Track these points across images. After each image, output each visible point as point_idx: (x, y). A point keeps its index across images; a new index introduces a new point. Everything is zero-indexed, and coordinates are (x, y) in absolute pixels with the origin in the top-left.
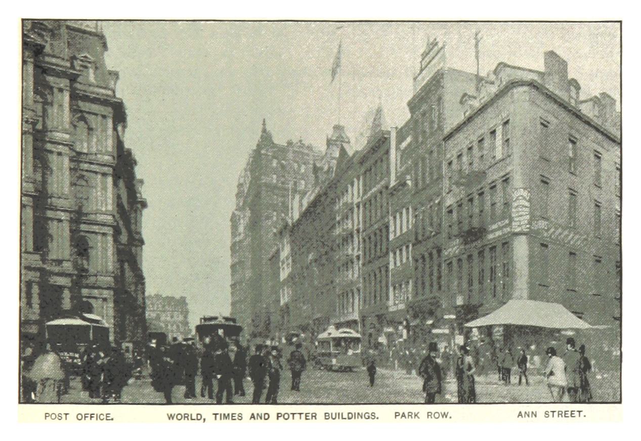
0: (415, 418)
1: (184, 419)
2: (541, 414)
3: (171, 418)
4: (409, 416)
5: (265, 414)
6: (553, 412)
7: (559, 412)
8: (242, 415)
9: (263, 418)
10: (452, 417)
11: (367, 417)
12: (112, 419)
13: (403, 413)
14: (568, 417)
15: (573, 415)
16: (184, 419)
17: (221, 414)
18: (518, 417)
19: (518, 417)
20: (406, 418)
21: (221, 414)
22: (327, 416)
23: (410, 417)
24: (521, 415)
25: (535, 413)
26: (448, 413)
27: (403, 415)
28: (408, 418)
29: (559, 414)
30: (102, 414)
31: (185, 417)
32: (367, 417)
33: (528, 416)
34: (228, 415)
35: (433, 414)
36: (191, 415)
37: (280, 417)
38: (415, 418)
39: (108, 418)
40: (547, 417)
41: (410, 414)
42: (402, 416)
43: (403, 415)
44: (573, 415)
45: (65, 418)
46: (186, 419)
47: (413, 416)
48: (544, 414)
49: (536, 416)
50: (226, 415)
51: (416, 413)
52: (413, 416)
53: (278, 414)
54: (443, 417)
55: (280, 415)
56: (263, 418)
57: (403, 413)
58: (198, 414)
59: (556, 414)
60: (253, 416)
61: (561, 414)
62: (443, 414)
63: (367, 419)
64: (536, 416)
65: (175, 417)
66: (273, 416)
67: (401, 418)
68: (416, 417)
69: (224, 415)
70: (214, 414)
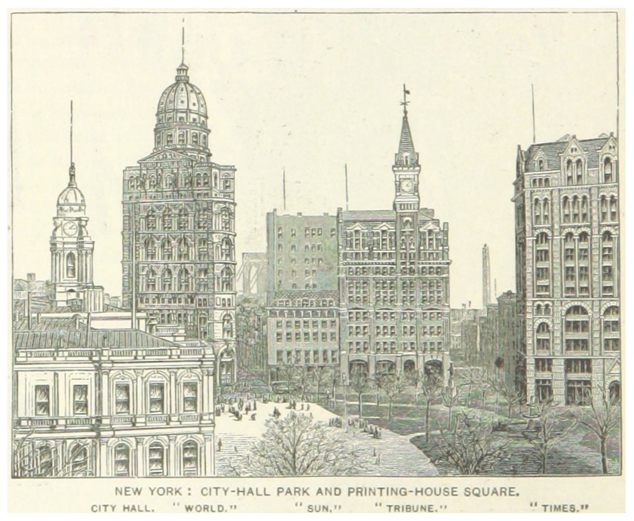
0: (303, 494)
1: (167, 494)
2: (460, 491)
3: (137, 493)
4: (295, 492)
5: (336, 489)
6: (381, 489)
7: (396, 506)
8: (465, 494)
9: (333, 493)
10: (520, 495)
11: (403, 494)
12: (518, 495)
13: (289, 489)
14: (129, 495)
15: (454, 493)
16: (167, 494)
17: (388, 489)
18: (317, 494)
19: (317, 494)
20: (497, 495)
21: (388, 489)
22: (468, 492)
23: (503, 494)
24: (321, 493)
25: (373, 491)
26: (141, 489)
27: (289, 491)
28: (501, 495)
29: (358, 492)
30: (94, 506)
31: (168, 492)
32: (403, 494)
33: (121, 493)
34: (560, 506)
35: (442, 494)
36: (212, 507)
37: (281, 492)
38: (303, 494)
39: (512, 493)
40: (447, 495)
41: (503, 491)
42: (287, 492)
43: (289, 491)
44: (454, 493)
45: (215, 494)
46: (170, 494)
47: (174, 492)
48: (307, 508)
49: (117, 489)
50: (557, 506)
51: (305, 489)
52: (174, 492)
53: (34, 274)
54: (135, 493)
55: (351, 490)
56: (333, 493)
57: (289, 489)
58: (219, 506)
59: (392, 508)
60: (320, 491)
61: (361, 492)
62: (135, 489)
63: (403, 495)
64: (117, 489)
65: (156, 490)
66: (460, 491)
67: (286, 494)
68: (178, 494)
69: (555, 506)
70: (388, 506)
